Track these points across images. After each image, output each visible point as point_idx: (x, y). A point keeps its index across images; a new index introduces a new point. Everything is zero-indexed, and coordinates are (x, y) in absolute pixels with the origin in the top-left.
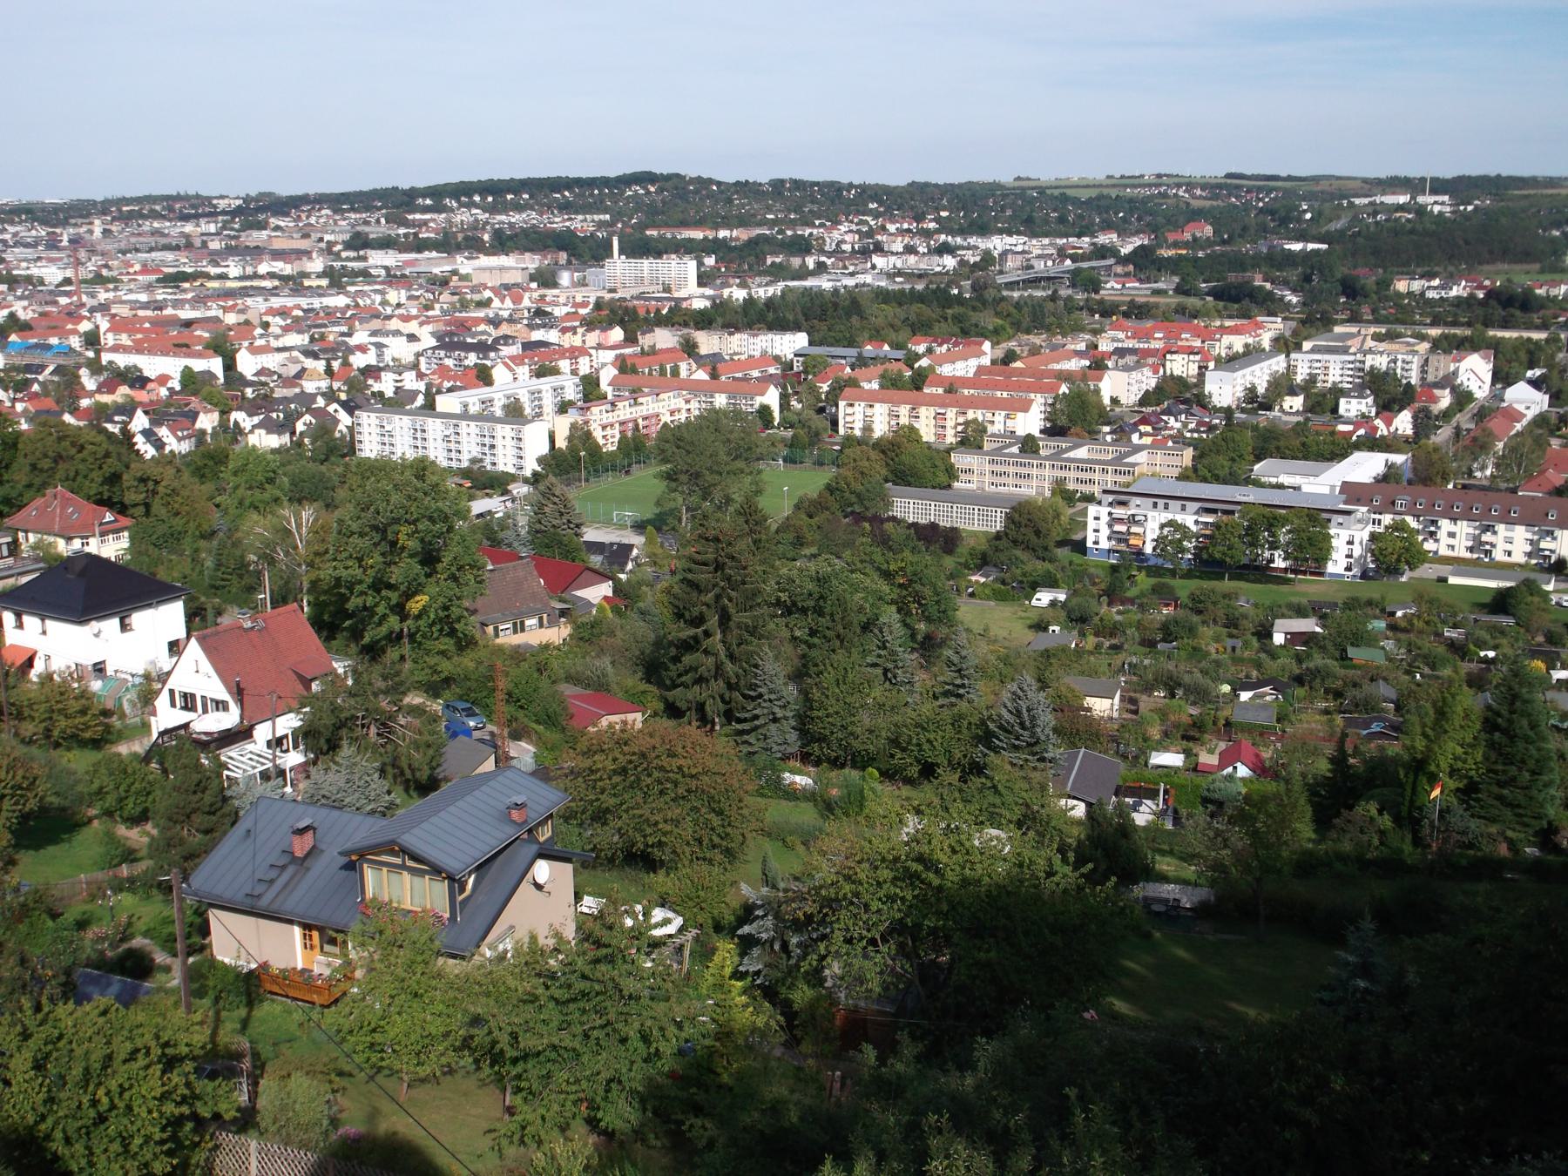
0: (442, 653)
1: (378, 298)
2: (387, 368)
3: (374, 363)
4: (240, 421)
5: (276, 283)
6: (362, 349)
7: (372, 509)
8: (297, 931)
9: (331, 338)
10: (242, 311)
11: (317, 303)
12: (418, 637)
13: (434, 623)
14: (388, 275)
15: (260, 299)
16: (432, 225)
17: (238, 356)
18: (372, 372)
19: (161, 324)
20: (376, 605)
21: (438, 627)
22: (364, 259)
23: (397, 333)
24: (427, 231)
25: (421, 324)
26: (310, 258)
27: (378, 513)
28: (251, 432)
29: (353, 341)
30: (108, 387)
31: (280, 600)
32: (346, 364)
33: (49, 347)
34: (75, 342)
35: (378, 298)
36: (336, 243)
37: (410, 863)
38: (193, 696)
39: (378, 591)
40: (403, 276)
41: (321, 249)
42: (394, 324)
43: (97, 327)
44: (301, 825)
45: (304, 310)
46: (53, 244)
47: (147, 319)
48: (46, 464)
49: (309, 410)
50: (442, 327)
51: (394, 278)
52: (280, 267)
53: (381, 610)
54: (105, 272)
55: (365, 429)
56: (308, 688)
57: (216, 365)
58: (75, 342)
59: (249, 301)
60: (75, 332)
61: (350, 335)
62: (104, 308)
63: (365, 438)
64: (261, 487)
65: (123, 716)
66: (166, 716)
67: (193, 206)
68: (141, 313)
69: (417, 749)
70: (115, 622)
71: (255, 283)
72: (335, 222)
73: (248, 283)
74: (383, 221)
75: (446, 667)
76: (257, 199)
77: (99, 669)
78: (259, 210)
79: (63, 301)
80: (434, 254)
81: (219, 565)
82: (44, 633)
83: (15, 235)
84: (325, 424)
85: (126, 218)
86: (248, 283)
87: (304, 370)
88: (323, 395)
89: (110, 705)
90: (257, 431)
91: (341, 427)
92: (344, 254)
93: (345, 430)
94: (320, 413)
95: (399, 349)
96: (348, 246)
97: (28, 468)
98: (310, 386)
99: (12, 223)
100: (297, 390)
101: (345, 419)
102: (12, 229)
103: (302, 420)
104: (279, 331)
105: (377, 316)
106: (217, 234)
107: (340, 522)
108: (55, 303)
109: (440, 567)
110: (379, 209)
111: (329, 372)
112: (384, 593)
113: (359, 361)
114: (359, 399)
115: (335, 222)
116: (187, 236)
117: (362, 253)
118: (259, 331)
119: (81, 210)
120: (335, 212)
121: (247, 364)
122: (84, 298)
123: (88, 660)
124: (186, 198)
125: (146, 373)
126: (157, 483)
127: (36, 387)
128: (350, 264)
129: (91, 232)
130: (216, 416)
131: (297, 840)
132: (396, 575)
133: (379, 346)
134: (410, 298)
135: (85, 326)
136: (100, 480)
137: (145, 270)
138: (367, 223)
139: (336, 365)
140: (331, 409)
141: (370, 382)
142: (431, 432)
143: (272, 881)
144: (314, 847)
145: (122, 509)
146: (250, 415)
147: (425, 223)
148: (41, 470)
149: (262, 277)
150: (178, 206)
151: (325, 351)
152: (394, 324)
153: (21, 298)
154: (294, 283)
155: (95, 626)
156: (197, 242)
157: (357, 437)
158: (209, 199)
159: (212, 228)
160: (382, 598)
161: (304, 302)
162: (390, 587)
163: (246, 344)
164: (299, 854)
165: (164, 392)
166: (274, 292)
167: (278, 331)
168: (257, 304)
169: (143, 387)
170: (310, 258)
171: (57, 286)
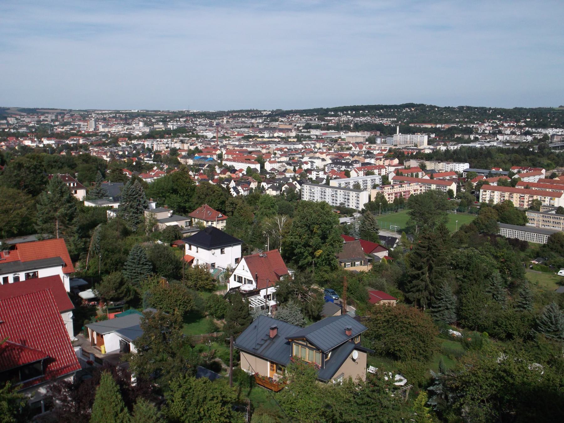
0: (326, 271)
1: (313, 146)
2: (314, 170)
3: (310, 168)
4: (264, 185)
5: (280, 140)
7: (306, 218)
8: (269, 363)
9: (296, 159)
10: (268, 149)
11: (292, 147)
13: (323, 260)
14: (317, 138)
15: (274, 145)
16: (333, 121)
17: (265, 164)
18: (309, 171)
19: (242, 152)
20: (305, 252)
21: (325, 262)
22: (309, 132)
23: (318, 158)
24: (331, 123)
25: (327, 155)
26: (291, 132)
27: (308, 220)
28: (267, 189)
29: (303, 160)
30: (223, 172)
31: (272, 247)
32: (300, 168)
33: (207, 158)
34: (215, 157)
35: (313, 146)
36: (300, 127)
37: (309, 345)
38: (242, 277)
39: (305, 247)
40: (322, 138)
41: (295, 129)
42: (318, 155)
43: (222, 152)
44: (273, 326)
45: (288, 149)
46: (211, 125)
47: (237, 150)
48: (203, 196)
49: (287, 183)
51: (319, 139)
52: (282, 134)
53: (306, 254)
54: (226, 135)
55: (305, 191)
56: (279, 279)
57: (258, 167)
58: (215, 157)
59: (270, 146)
60: (215, 154)
61: (302, 158)
62: (225, 146)
63: (305, 194)
64: (269, 208)
65: (219, 282)
66: (233, 284)
67: (255, 114)
68: (236, 148)
69: (314, 305)
70: (220, 250)
71: (273, 140)
72: (301, 119)
73: (271, 140)
74: (317, 119)
76: (276, 112)
77: (213, 265)
78: (276, 115)
79: (213, 144)
80: (333, 131)
81: (253, 234)
82: (197, 252)
83: (200, 122)
84: (292, 187)
85: (234, 117)
86: (271, 140)
87: (286, 169)
88: (292, 178)
89: (215, 278)
90: (269, 189)
91: (297, 189)
92: (303, 131)
93: (298, 191)
94: (290, 185)
95: (318, 163)
96: (304, 128)
97: (197, 198)
98: (288, 175)
99: (199, 118)
100: (284, 176)
101: (298, 187)
102: (199, 120)
103: (284, 187)
104: (279, 156)
105: (312, 152)
106: (262, 123)
107: (294, 222)
108: (210, 144)
109: (327, 240)
110: (316, 115)
111: (295, 170)
113: (305, 167)
114: (304, 180)
115: (301, 119)
116: (252, 123)
117: (309, 130)
118: (273, 156)
119: (220, 114)
120: (301, 116)
121: (268, 167)
122: (219, 143)
123: (210, 262)
124: (253, 111)
125: (236, 168)
126: (236, 205)
127: (202, 171)
129: (223, 121)
130: (256, 183)
131: (271, 332)
133: (312, 162)
135: (218, 152)
136: (218, 203)
137: (238, 134)
138: (311, 120)
139: (297, 168)
140: (294, 183)
141: (308, 174)
142: (327, 193)
143: (262, 345)
144: (277, 335)
145: (224, 213)
146: (268, 184)
147: (331, 120)
148: (201, 199)
149: (275, 138)
150: (250, 113)
151: (293, 163)
152: (318, 155)
153: (200, 142)
154: (286, 140)
155: (213, 251)
156: (256, 126)
157: (302, 193)
158: (261, 111)
159: (261, 121)
161: (288, 146)
162: (309, 246)
163: (268, 160)
164: (272, 336)
165: (241, 175)
166: (278, 143)
167: (279, 156)
168: (273, 147)
169: (234, 173)
170: (291, 132)
171: (211, 139)
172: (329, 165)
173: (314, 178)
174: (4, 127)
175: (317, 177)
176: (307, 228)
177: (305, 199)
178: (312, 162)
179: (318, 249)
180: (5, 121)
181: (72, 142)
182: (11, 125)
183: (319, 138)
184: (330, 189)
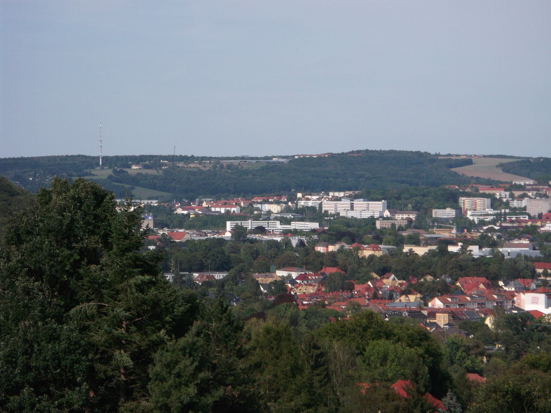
174: (445, 235)
180: (449, 213)
181: (405, 234)
182: (471, 225)
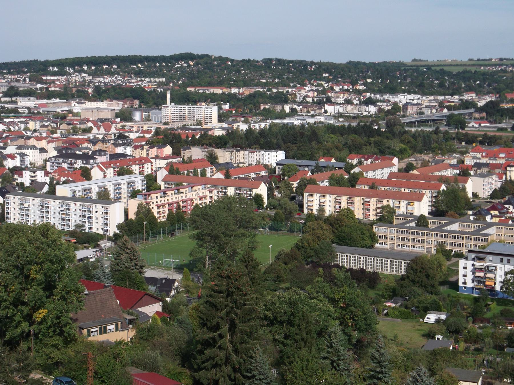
0: (55, 346)
1: (23, 126)
2: (26, 169)
3: (18, 165)
6: (12, 157)
7: (15, 255)
12: (40, 336)
13: (50, 327)
14: (30, 112)
16: (57, 83)
18: (17, 171)
20: (14, 315)
21: (53, 329)
22: (15, 102)
23: (34, 147)
25: (48, 142)
27: (19, 258)
35: (23, 126)
40: (39, 113)
42: (32, 142)
50: (61, 144)
51: (33, 114)
53: (18, 318)
55: (12, 206)
63: (11, 211)
73: (7, 115)
74: (28, 80)
75: (57, 355)
80: (58, 100)
105: (21, 137)
110: (26, 73)
112: (20, 307)
113: (9, 164)
114: (9, 187)
117: (14, 99)
128: (6, 106)
132: (28, 296)
133: (22, 155)
134: (42, 126)
138: (18, 81)
141: (16, 177)
142: (52, 208)
147: (53, 81)
152: (32, 142)
157: (7, 210)
160: (18, 311)
162: (24, 304)
172: (53, 159)
173: (27, 184)
175: (32, 181)
176: (18, 273)
177: (12, 221)
178: (22, 155)
179: (39, 308)
183: (34, 113)
184: (57, 201)
